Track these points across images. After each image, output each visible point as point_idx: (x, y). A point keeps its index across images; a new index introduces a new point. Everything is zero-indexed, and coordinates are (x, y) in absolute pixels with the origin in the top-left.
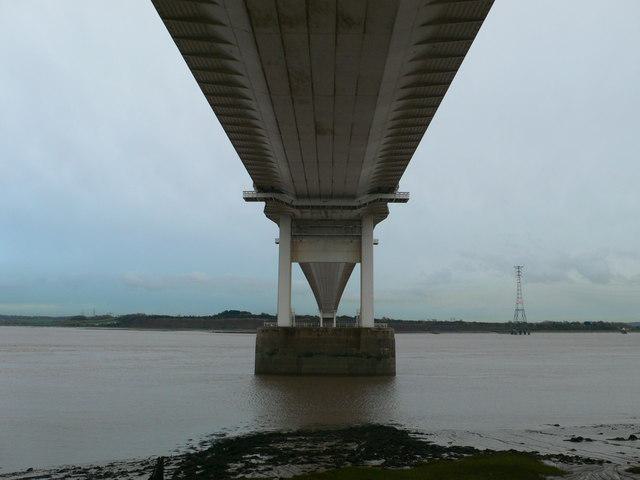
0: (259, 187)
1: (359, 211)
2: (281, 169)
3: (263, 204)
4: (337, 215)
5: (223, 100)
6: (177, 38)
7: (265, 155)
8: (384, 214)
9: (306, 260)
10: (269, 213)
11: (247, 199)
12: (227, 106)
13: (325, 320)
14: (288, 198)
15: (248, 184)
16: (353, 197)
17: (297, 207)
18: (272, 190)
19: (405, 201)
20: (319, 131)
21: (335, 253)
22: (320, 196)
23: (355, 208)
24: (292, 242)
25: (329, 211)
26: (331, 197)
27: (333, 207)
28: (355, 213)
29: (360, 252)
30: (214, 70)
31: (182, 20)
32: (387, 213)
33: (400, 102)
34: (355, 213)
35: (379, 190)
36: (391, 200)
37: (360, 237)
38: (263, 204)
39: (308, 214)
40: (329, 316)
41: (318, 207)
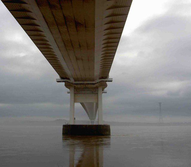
0: (62, 78)
1: (97, 84)
2: (69, 72)
3: (64, 83)
4: (89, 86)
5: (44, 50)
6: (16, 18)
7: (57, 60)
8: (106, 86)
9: (83, 102)
10: (66, 86)
11: (58, 82)
12: (53, 62)
13: (91, 122)
14: (72, 81)
15: (58, 77)
16: (94, 80)
17: (75, 84)
18: (66, 78)
19: (111, 81)
20: (77, 59)
21: (89, 99)
22: (82, 80)
23: (94, 84)
24: (74, 96)
25: (87, 85)
26: (86, 80)
27: (87, 84)
28: (95, 86)
29: (98, 98)
30: (45, 51)
31: (22, 18)
32: (107, 85)
33: (106, 25)
34: (95, 86)
35: (102, 78)
36: (107, 81)
37: (97, 94)
38: (64, 83)
39: (79, 86)
40: (93, 121)
41: (82, 84)
